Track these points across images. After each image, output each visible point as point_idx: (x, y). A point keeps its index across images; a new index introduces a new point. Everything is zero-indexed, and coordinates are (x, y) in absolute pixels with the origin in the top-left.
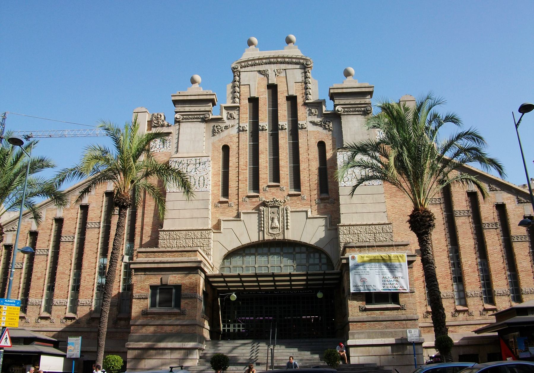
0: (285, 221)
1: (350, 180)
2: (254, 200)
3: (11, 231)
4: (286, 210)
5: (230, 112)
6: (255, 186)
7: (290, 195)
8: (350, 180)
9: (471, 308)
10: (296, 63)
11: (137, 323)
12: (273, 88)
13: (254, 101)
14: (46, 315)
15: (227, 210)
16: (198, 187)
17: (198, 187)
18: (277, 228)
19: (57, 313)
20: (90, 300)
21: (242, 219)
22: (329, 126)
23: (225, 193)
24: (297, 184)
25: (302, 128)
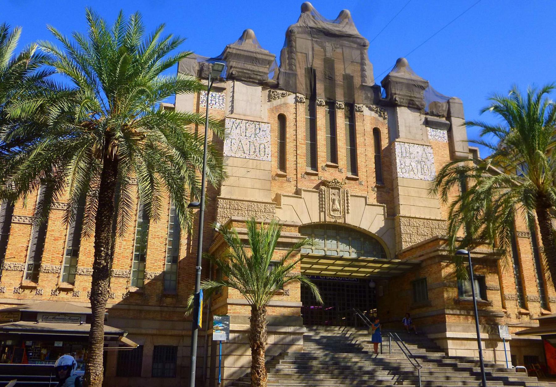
0: (346, 205)
1: (407, 172)
2: (313, 178)
4: (347, 194)
6: (314, 164)
7: (348, 178)
8: (407, 172)
9: (509, 311)
14: (66, 285)
16: (258, 155)
17: (258, 155)
18: (338, 211)
19: (82, 284)
20: (128, 271)
21: (302, 196)
22: (384, 114)
23: (282, 165)
24: (354, 168)
25: (359, 111)
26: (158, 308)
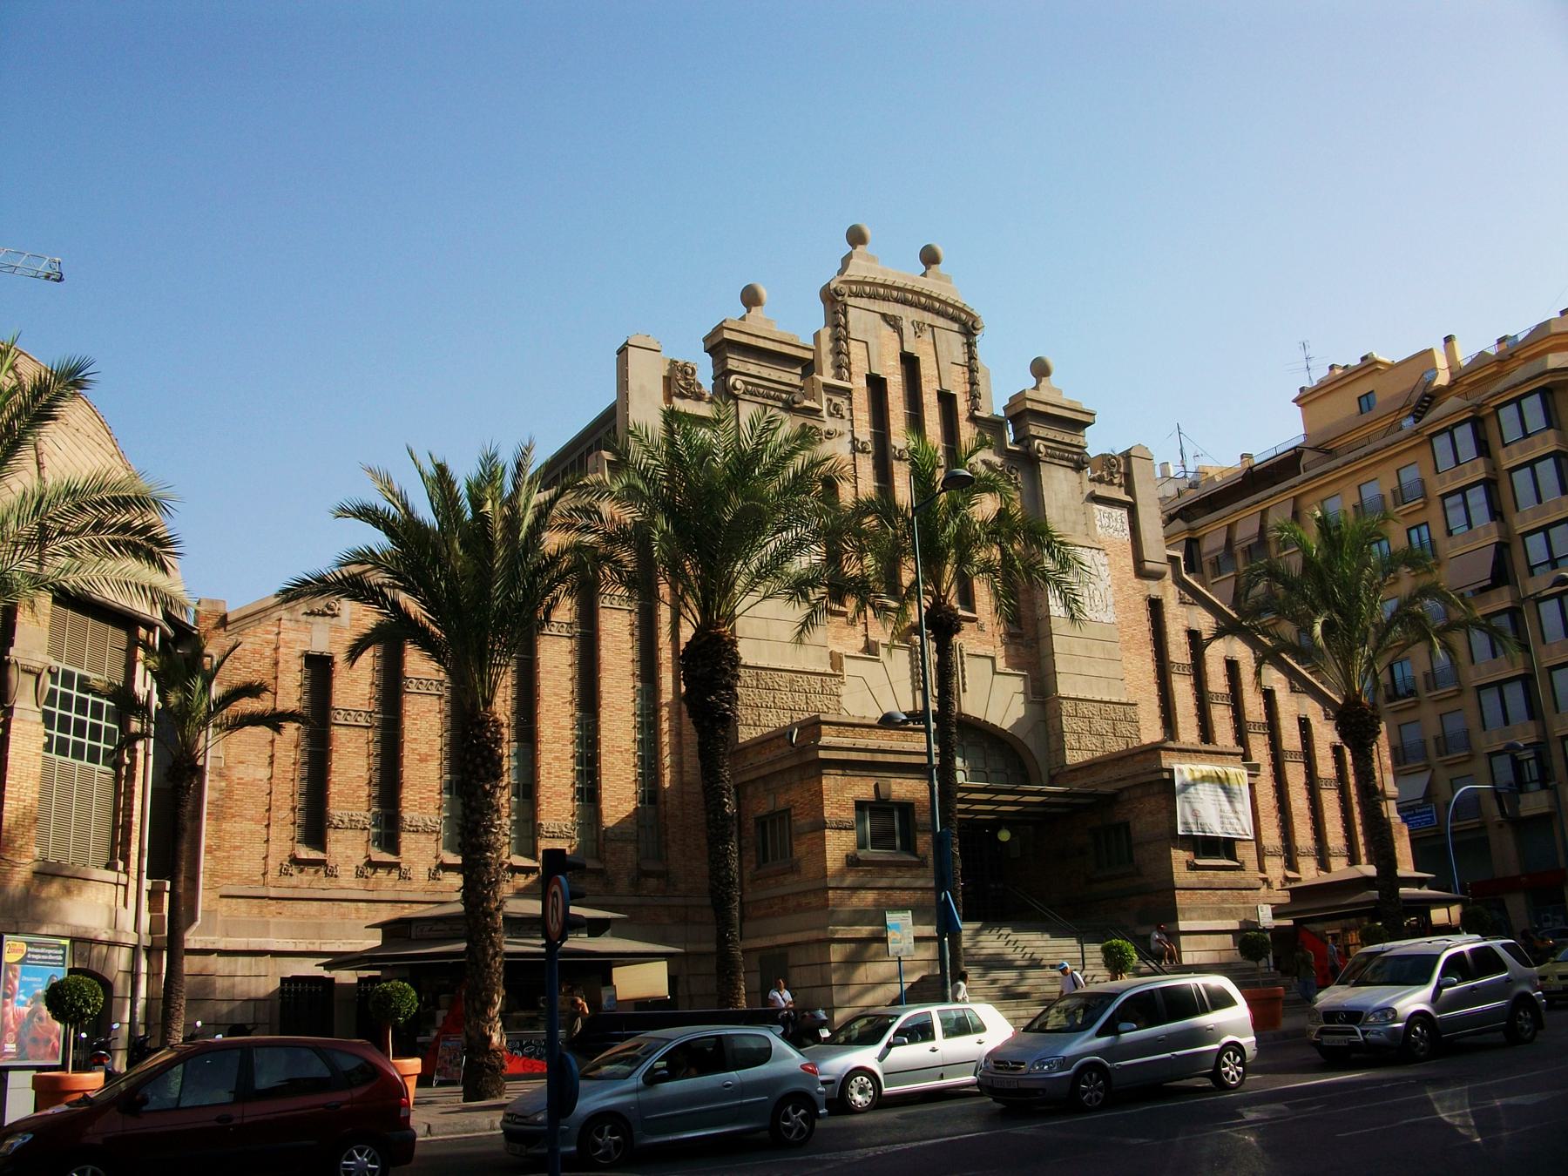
3: (324, 614)
5: (836, 400)
10: (953, 319)
11: (845, 884)
12: (910, 363)
13: (877, 385)
15: (845, 632)
26: (635, 900)
